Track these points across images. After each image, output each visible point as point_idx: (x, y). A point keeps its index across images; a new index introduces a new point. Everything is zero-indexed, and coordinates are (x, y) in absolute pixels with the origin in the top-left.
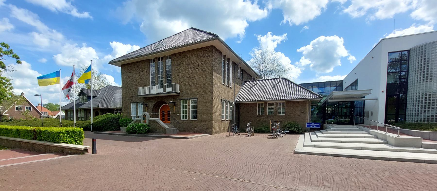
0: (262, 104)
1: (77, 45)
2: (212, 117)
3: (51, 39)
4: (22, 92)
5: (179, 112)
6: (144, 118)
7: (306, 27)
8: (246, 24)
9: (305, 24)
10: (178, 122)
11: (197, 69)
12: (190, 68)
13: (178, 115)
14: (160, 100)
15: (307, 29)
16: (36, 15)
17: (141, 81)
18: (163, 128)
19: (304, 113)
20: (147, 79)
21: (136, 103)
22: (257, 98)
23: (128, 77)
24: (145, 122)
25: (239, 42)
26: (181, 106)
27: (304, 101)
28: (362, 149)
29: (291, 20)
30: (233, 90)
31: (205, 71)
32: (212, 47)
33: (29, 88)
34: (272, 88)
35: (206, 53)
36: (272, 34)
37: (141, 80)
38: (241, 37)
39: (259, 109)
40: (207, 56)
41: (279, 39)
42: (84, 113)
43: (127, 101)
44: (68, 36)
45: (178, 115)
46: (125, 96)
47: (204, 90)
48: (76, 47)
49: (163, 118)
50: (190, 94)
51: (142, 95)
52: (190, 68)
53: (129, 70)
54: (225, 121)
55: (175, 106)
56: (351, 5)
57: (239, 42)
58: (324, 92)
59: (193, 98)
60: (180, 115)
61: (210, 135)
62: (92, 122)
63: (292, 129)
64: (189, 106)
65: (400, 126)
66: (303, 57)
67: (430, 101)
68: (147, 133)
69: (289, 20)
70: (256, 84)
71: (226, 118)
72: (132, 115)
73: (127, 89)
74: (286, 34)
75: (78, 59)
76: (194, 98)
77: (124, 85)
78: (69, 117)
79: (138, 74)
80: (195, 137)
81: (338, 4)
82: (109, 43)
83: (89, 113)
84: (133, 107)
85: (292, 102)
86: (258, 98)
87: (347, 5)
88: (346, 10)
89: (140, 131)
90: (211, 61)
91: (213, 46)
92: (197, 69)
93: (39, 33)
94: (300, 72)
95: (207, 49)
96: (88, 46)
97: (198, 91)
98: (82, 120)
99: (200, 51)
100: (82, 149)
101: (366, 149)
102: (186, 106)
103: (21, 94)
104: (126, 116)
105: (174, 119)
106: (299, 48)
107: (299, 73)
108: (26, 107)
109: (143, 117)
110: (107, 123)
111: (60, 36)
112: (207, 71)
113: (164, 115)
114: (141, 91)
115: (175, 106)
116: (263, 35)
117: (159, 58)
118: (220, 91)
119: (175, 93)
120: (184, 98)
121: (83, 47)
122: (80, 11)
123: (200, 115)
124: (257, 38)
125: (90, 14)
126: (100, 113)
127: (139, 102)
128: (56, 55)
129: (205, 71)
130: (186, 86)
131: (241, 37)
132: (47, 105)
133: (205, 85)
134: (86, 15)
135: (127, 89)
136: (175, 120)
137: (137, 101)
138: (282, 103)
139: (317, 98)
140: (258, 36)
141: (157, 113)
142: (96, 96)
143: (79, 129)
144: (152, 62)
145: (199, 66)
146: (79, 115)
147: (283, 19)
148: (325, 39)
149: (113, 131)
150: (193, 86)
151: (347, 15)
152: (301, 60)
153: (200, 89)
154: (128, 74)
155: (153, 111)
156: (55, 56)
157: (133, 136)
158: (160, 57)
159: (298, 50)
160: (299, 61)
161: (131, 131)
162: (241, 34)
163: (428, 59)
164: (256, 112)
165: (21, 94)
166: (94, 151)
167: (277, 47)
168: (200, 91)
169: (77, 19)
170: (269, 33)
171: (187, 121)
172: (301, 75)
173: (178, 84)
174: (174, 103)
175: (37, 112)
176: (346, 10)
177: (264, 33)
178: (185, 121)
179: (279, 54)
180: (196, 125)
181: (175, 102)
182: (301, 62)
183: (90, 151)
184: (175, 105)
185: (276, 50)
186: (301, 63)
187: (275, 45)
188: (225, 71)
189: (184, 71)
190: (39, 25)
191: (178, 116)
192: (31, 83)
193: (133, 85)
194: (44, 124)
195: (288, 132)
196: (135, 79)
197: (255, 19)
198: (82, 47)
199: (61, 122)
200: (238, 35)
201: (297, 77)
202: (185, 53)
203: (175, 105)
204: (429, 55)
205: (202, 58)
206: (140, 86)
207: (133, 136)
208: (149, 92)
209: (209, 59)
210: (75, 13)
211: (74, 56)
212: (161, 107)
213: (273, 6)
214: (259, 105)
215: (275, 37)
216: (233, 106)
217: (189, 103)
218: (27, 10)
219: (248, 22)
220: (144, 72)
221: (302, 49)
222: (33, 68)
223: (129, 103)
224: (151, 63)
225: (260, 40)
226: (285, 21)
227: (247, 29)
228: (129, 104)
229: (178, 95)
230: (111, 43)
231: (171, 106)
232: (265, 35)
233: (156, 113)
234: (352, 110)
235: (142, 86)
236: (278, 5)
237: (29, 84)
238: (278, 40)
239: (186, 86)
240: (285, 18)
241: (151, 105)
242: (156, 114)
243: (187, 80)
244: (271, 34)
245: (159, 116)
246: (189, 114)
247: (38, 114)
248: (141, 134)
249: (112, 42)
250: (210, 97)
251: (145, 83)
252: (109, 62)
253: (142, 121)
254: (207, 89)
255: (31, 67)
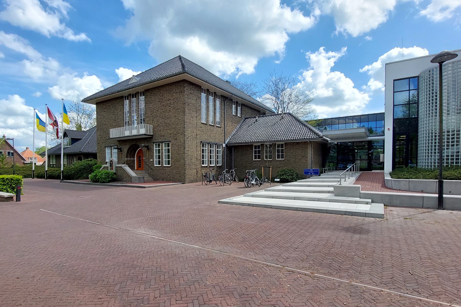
0: (259, 146)
1: (76, 74)
2: (184, 163)
3: (45, 68)
4: (4, 135)
5: (152, 157)
6: (111, 165)
7: (368, 38)
8: (285, 38)
9: (365, 34)
10: (152, 169)
11: (170, 106)
12: (163, 105)
13: (151, 160)
14: (134, 143)
15: (369, 40)
16: (26, 41)
17: (115, 122)
18: (129, 176)
19: (305, 157)
20: (121, 118)
21: (110, 146)
22: (291, 137)
23: (102, 117)
24: (112, 169)
25: (277, 62)
26: (154, 150)
27: (305, 142)
28: (295, 198)
29: (345, 30)
30: (222, 129)
31: (178, 109)
32: (184, 81)
33: (24, 128)
34: (272, 126)
35: (178, 89)
36: (326, 49)
37: (115, 120)
38: (281, 55)
39: (278, 151)
40: (179, 92)
41: (335, 56)
42: (67, 159)
43: (102, 145)
44: (65, 63)
45: (151, 160)
46: (99, 139)
47: (177, 132)
48: (76, 76)
49: (139, 165)
50: (164, 136)
51: (112, 137)
52: (163, 105)
53: (103, 109)
54: (209, 167)
55: (149, 150)
56: (432, 4)
57: (277, 62)
58: (376, 128)
59: (166, 141)
60: (153, 161)
61: (182, 184)
62: (62, 169)
63: (284, 177)
64: (162, 150)
65: (79, 177)
66: (372, 80)
67: (447, 141)
68: (112, 182)
69: (342, 30)
70: (282, 118)
71: (211, 164)
72: (106, 161)
73: (102, 131)
74: (345, 48)
75: (79, 91)
76: (167, 141)
77: (98, 126)
78: (52, 164)
79: (112, 113)
80: (156, 186)
81: (410, 5)
82: (115, 71)
83: (71, 159)
84: (108, 151)
85: (291, 143)
86: (293, 137)
87: (424, 5)
88: (423, 12)
89: (102, 179)
90: (183, 97)
91: (184, 80)
92: (170, 106)
93: (31, 61)
94: (369, 99)
95: (179, 84)
96: (90, 75)
97: (171, 132)
98: (53, 167)
99: (172, 86)
100: (5, 197)
101: (302, 199)
102: (159, 150)
103: (3, 136)
104: (101, 163)
105: (148, 165)
106: (362, 69)
107: (367, 100)
108: (8, 152)
109: (110, 163)
110: (80, 171)
111: (54, 64)
112: (179, 109)
113: (140, 161)
114: (114, 133)
115: (149, 150)
116: (313, 52)
117: (133, 95)
118: (198, 132)
119: (148, 135)
120: (157, 141)
121: (84, 76)
122: (76, 34)
123: (173, 161)
124: (305, 55)
125: (87, 35)
126: (83, 158)
127: (155, 143)
128: (52, 86)
129: (178, 109)
130: (159, 127)
131: (281, 55)
132: (40, 148)
133: (177, 125)
134: (83, 36)
135: (102, 131)
136: (149, 166)
137: (112, 145)
138: (281, 144)
139: (317, 138)
140: (306, 53)
141: (132, 158)
142: (80, 139)
143: (16, 176)
144: (133, 98)
145: (172, 103)
146: (51, 161)
147: (335, 29)
148: (399, 52)
149: (85, 179)
150: (166, 126)
151: (425, 17)
152: (369, 84)
153: (173, 130)
154: (103, 113)
155: (128, 156)
156: (51, 89)
157: (96, 185)
158: (140, 92)
159: (361, 71)
160: (366, 85)
161: (94, 180)
162: (279, 52)
163: (436, 90)
164: (252, 156)
165: (3, 136)
166: (18, 199)
167: (334, 66)
168: (173, 133)
169: (73, 42)
170: (322, 49)
171: (160, 168)
172: (370, 102)
173: (152, 124)
174: (147, 147)
175: (20, 158)
176: (423, 12)
177: (315, 50)
178: (158, 168)
179: (338, 75)
180: (169, 173)
181: (149, 146)
182: (369, 86)
183: (15, 198)
184: (121, 151)
185: (333, 69)
186: (371, 87)
187: (332, 62)
188: (208, 107)
189: (157, 109)
190: (30, 52)
191: (151, 161)
192: (25, 122)
193: (108, 126)
194: (15, 172)
195: (279, 180)
196: (110, 119)
197: (297, 30)
198: (83, 76)
199: (46, 169)
200: (276, 53)
201: (364, 106)
202: (158, 88)
203: (148, 149)
204: (437, 86)
205: (174, 94)
206: (114, 127)
207: (96, 185)
208: (124, 134)
209: (181, 96)
210: (70, 36)
211: (73, 88)
212: (136, 153)
213: (322, 11)
214: (255, 146)
215: (331, 54)
216: (222, 149)
217: (162, 146)
218: (17, 36)
219: (289, 35)
220: (118, 111)
221: (366, 68)
222: (27, 103)
223: (104, 147)
224: (133, 99)
225: (310, 59)
226: (337, 33)
227: (287, 44)
228: (103, 148)
229: (152, 138)
230: (116, 70)
231: (144, 149)
232: (317, 52)
233: (132, 159)
234: (369, 152)
235: (117, 127)
236: (328, 10)
237: (23, 123)
238: (335, 57)
239: (159, 127)
240: (337, 29)
241: (125, 149)
242: (131, 160)
243: (160, 120)
244: (324, 50)
245: (135, 162)
246: (162, 159)
247: (21, 160)
248: (104, 182)
249: (118, 69)
250: (182, 139)
251: (119, 124)
252: (82, 100)
253: (109, 168)
254: (179, 130)
255: (25, 102)
